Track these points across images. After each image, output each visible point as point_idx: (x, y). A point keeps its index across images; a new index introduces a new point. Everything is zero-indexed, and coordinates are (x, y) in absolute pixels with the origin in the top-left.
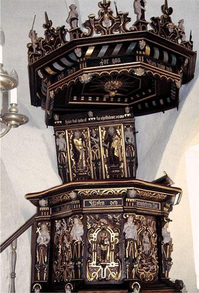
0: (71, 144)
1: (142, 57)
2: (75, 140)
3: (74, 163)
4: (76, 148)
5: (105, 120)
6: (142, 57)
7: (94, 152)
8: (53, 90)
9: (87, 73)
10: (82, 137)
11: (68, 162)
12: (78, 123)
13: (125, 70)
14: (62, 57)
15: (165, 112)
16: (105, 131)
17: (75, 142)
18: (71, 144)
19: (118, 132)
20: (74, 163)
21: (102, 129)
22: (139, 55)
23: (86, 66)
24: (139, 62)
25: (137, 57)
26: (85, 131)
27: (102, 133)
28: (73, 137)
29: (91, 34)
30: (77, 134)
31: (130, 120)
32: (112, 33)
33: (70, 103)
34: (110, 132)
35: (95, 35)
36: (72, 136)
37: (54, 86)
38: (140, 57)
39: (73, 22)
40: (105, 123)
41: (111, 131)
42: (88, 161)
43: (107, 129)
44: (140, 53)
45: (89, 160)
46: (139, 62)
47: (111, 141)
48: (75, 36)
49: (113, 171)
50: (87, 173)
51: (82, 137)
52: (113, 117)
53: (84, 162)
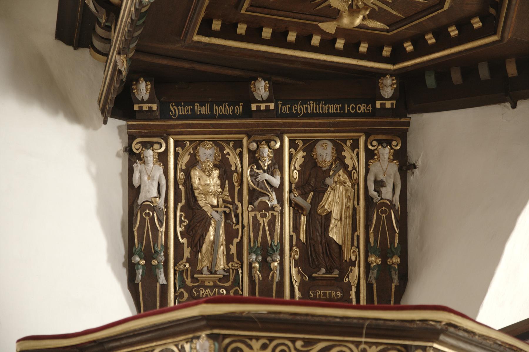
3: (187, 253)
4: (195, 198)
5: (307, 115)
7: (261, 221)
11: (166, 247)
15: (522, 105)
16: (301, 154)
19: (348, 161)
20: (187, 253)
21: (293, 144)
27: (291, 157)
30: (207, 154)
31: (391, 123)
41: (325, 153)
42: (234, 249)
45: (240, 245)
47: (320, 191)
49: (320, 293)
50: (228, 290)
52: (333, 108)
53: (222, 250)
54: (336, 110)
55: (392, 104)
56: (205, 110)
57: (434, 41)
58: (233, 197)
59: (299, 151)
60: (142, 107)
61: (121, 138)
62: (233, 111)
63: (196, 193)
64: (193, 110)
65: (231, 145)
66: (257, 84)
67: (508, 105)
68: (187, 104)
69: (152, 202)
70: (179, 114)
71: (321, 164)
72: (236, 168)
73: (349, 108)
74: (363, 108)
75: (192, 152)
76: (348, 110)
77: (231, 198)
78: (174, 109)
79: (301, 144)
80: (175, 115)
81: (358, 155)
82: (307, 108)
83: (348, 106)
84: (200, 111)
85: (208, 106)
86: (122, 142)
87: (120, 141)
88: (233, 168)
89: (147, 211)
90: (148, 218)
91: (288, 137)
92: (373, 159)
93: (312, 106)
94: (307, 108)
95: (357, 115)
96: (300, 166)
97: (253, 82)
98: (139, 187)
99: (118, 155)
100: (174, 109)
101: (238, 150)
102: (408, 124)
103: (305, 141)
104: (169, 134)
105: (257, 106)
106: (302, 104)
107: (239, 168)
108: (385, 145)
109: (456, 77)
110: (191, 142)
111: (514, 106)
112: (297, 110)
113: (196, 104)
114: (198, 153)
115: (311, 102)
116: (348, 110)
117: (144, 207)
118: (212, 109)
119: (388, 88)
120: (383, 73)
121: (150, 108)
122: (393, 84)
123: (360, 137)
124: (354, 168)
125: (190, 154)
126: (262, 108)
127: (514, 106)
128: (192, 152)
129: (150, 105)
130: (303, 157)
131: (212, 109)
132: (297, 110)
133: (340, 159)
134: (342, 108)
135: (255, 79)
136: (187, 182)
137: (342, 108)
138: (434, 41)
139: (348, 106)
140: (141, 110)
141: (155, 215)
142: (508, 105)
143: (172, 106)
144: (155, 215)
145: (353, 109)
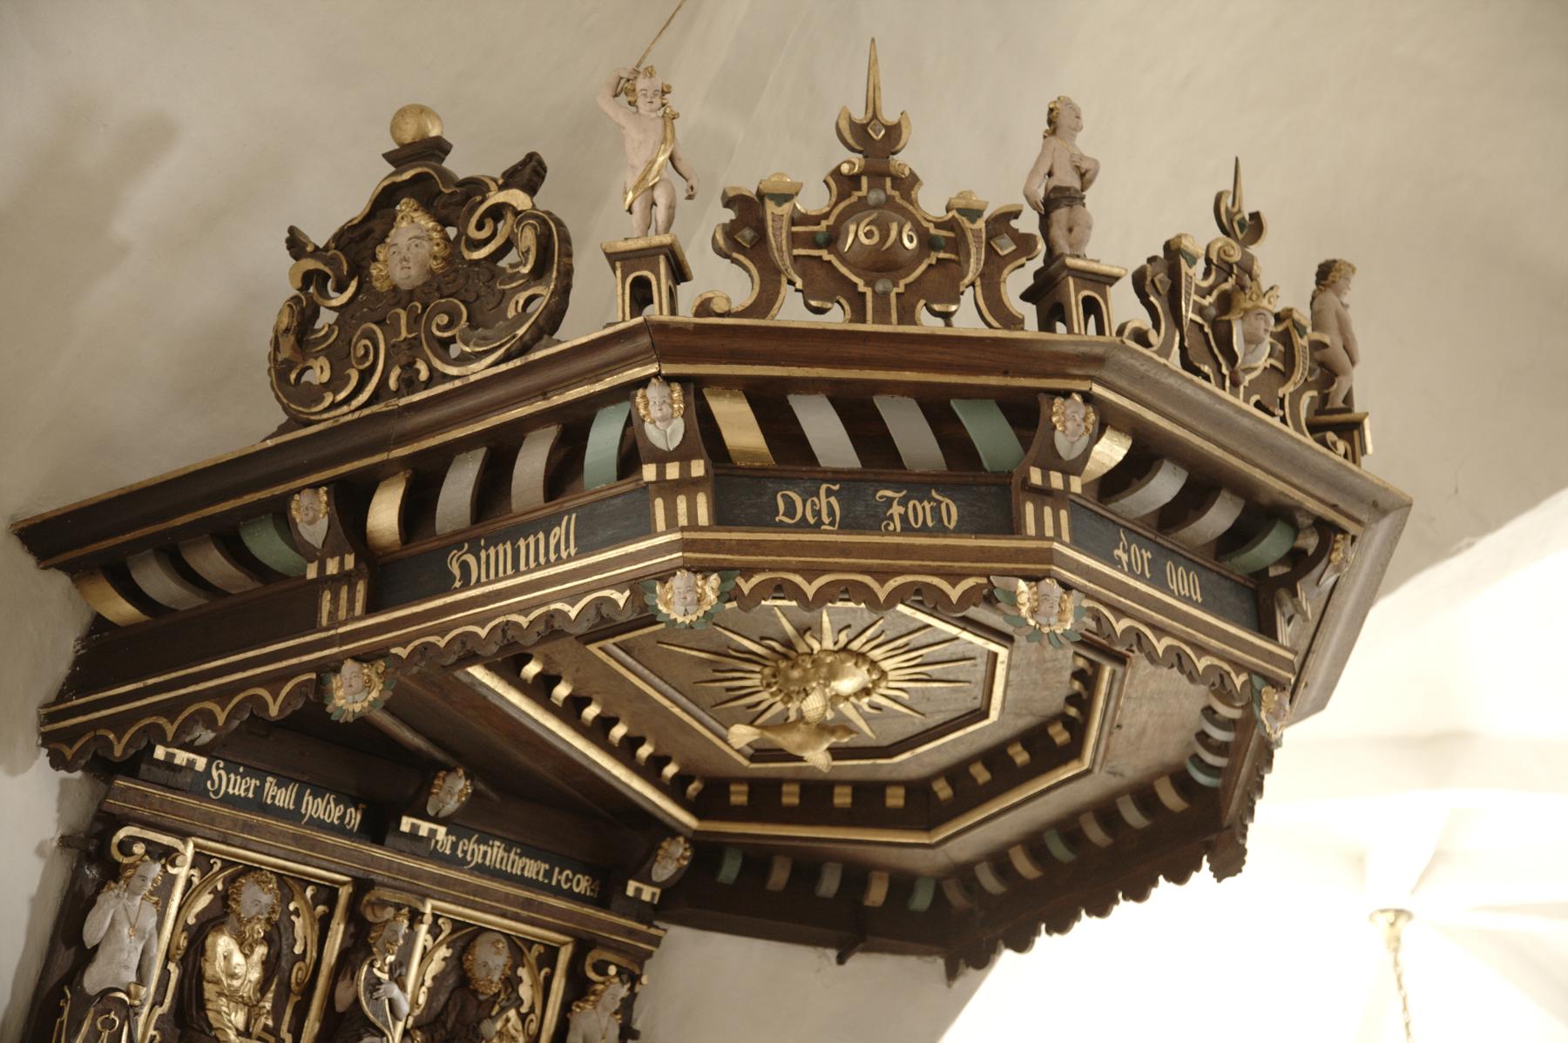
0: (172, 966)
1: (1064, 514)
2: (223, 944)
4: (201, 1004)
5: (481, 870)
6: (1064, 514)
8: (725, 571)
9: (1067, 587)
10: (277, 936)
12: (294, 816)
13: (1226, 667)
14: (727, 384)
15: (858, 962)
16: (444, 952)
17: (220, 963)
18: (172, 966)
19: (525, 991)
22: (1043, 494)
23: (1066, 537)
24: (676, 536)
25: (1029, 508)
26: (316, 900)
27: (426, 954)
28: (218, 917)
29: (766, 301)
30: (256, 899)
31: (631, 933)
32: (907, 315)
33: (478, 672)
34: (479, 973)
35: (791, 311)
36: (205, 900)
37: (741, 547)
38: (1048, 511)
39: (1060, 215)
40: (478, 891)
41: (491, 961)
43: (465, 938)
44: (1056, 480)
46: (676, 536)
48: (641, 294)
51: (277, 936)
52: (532, 868)
54: (247, 790)
55: (654, 895)
56: (283, 797)
57: (795, 800)
58: (278, 1018)
59: (440, 944)
60: (174, 755)
61: (59, 810)
62: (342, 818)
63: (209, 990)
64: (259, 790)
65: (309, 892)
66: (450, 780)
67: (832, 954)
68: (252, 771)
69: (128, 993)
70: (226, 792)
71: (481, 985)
72: (305, 951)
73: (561, 877)
74: (582, 885)
75: (220, 887)
76: (559, 881)
77: (274, 1020)
78: (220, 776)
79: (447, 929)
80: (216, 792)
81: (548, 980)
82: (485, 853)
83: (560, 873)
84: (273, 797)
85: (293, 789)
86: (60, 821)
87: (55, 815)
88: (298, 950)
89: (112, 1015)
90: (105, 1035)
91: (196, 846)
92: (117, 882)
93: (495, 853)
94: (485, 853)
95: (570, 895)
96: (434, 978)
97: (441, 774)
98: (96, 948)
99: (40, 851)
100: (220, 776)
101: (321, 909)
102: (656, 941)
103: (227, 864)
104: (190, 835)
105: (413, 825)
106: (478, 842)
107: (312, 954)
108: (625, 977)
109: (779, 876)
110: (227, 864)
111: (841, 960)
112: (465, 852)
113: (270, 779)
114: (239, 893)
115: (497, 843)
116: (559, 881)
117: (83, 1001)
118: (298, 801)
119: (671, 861)
120: (669, 830)
121: (191, 763)
122: (684, 858)
123: (565, 944)
124: (532, 1010)
125: (215, 891)
126: (177, 761)
127: (841, 960)
128: (220, 887)
129: (192, 756)
130: (445, 959)
131: (298, 801)
132: (465, 852)
133: (512, 982)
134: (548, 874)
135: (450, 770)
136: (191, 959)
137: (548, 874)
138: (795, 800)
139: (560, 873)
140: (168, 764)
141: (126, 1029)
142: (832, 954)
143: (218, 768)
144: (126, 1029)
145: (568, 880)
